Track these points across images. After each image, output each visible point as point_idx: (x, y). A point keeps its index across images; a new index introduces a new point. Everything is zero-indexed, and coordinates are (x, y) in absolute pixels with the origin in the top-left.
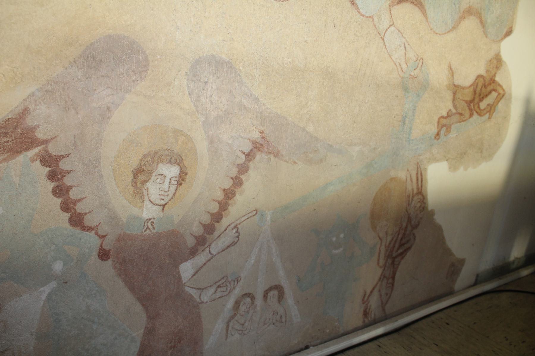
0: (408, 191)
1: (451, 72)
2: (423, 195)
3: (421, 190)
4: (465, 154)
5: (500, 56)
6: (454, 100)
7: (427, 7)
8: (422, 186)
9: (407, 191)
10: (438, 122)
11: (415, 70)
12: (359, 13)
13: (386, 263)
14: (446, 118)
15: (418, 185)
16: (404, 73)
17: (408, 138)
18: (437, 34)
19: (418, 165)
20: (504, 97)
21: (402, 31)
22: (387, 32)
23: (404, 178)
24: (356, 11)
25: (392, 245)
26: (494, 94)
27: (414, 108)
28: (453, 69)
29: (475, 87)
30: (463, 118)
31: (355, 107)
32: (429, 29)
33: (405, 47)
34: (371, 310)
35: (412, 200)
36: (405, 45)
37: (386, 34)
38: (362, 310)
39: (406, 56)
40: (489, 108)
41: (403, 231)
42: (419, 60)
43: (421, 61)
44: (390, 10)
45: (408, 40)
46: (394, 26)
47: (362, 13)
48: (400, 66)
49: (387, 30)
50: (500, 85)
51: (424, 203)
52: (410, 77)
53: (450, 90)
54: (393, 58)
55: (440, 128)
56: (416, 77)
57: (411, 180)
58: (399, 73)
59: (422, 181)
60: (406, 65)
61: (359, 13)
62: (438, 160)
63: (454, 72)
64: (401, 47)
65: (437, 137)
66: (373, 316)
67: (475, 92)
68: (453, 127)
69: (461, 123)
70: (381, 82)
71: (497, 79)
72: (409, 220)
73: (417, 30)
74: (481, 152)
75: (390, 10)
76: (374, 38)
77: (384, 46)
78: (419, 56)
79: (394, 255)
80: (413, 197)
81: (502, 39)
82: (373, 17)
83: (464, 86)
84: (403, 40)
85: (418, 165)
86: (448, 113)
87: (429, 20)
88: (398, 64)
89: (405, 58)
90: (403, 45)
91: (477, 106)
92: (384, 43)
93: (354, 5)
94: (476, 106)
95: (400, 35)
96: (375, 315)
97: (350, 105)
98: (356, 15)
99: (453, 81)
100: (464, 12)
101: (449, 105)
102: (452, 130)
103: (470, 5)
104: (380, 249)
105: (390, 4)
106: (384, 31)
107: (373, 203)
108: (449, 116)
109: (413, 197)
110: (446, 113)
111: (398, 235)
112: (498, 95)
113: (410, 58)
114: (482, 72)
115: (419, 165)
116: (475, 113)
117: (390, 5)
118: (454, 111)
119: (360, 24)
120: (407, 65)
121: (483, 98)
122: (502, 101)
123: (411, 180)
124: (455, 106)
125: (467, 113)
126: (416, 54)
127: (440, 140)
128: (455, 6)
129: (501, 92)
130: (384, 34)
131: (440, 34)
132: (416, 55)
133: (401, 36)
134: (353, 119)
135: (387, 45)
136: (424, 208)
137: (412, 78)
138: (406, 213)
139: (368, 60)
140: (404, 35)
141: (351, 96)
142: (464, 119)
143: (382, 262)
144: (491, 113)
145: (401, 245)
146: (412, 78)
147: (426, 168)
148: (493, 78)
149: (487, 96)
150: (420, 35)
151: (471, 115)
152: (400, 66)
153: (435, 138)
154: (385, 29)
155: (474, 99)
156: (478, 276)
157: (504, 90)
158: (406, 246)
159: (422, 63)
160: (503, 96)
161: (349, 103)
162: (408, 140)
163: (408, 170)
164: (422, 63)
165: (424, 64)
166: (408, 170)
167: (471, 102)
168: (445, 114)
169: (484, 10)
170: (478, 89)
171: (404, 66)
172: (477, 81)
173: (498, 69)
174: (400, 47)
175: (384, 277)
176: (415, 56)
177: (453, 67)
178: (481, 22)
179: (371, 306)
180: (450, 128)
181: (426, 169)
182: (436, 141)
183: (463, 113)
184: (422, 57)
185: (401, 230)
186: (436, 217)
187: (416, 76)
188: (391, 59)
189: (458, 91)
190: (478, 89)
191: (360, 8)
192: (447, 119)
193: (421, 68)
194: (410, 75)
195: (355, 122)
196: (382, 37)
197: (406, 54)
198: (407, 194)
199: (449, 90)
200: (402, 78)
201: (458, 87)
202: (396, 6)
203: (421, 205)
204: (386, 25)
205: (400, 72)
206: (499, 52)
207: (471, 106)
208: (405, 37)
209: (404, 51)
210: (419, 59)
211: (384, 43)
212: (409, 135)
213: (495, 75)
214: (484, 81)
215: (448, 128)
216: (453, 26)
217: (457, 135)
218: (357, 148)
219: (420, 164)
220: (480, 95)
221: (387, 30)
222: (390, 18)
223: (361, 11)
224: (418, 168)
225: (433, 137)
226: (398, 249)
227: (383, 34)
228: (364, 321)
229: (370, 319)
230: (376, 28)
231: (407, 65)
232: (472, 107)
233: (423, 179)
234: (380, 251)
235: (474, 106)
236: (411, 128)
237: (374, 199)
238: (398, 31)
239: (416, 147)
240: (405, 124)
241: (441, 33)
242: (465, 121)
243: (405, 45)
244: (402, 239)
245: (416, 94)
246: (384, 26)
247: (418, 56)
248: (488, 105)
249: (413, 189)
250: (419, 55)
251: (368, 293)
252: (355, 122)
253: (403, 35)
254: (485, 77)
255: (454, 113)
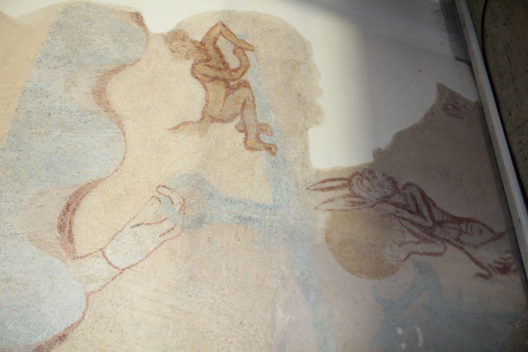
0: (346, 206)
1: (181, 128)
2: (353, 176)
3: (345, 179)
4: (299, 95)
5: (169, 33)
6: (223, 121)
7: (83, 181)
8: (341, 179)
9: (346, 208)
10: (252, 149)
11: (173, 203)
12: (79, 322)
13: (440, 239)
14: (247, 135)
15: (338, 187)
16: (175, 225)
17: (271, 209)
18: (124, 158)
19: (311, 189)
20: (226, 24)
21: (114, 232)
22: (113, 262)
23: (328, 214)
24: (76, 330)
25: (417, 230)
26: (222, 43)
27: (229, 202)
28: (178, 123)
29: (207, 79)
30: (249, 100)
31: (218, 323)
32: (116, 174)
33: (138, 225)
34: (501, 261)
35: (358, 196)
36: (134, 226)
37: (116, 265)
38: (499, 276)
39: (151, 222)
40: (239, 51)
41: (400, 210)
42: (160, 193)
43: (160, 189)
44: (81, 257)
45: (128, 219)
46: (105, 247)
47: (81, 316)
48: (164, 234)
49: (110, 263)
50: (208, 34)
51: (363, 172)
52: (182, 212)
53: (208, 128)
54: (152, 248)
55: (261, 145)
56: (184, 200)
57: (330, 201)
58: (175, 237)
59: (334, 180)
60: (164, 223)
61: (79, 322)
62: (306, 148)
63: (182, 121)
64: (137, 233)
65: (273, 150)
66: (508, 255)
67: (215, 79)
68: (260, 121)
69: (257, 106)
70: (186, 273)
71: (199, 38)
72: (385, 200)
73: (115, 201)
74: (298, 64)
75: (81, 257)
76: (120, 289)
77: (133, 268)
78: (153, 195)
79: (430, 223)
80: (354, 195)
81: (146, 30)
82: (88, 294)
83: (204, 102)
84: (127, 229)
85: (311, 189)
86: (241, 131)
87: (103, 177)
88: (161, 239)
89: (154, 224)
90: (134, 229)
91: (233, 74)
92: (128, 268)
93: (66, 336)
94: (235, 75)
95: (118, 237)
96: (507, 252)
97: (215, 334)
98: (82, 329)
99: (196, 122)
100: (99, 104)
101: (230, 128)
102: (265, 122)
103: (91, 92)
104: (420, 254)
105: (72, 258)
106: (111, 268)
107: (358, 274)
108: (244, 130)
109: (354, 195)
110: (241, 134)
111: (404, 219)
112: (222, 35)
113: (155, 213)
114: (187, 65)
115: (311, 186)
116: (243, 78)
117: (73, 259)
118: (238, 119)
119: (97, 321)
120: (164, 220)
121: (224, 63)
122: (231, 27)
123: (330, 201)
124: (230, 120)
125: (243, 93)
126: (150, 201)
127: (278, 145)
128: (89, 121)
129: (218, 30)
130: (116, 267)
131: (126, 152)
132: (152, 202)
133: (121, 235)
134: (236, 327)
135: (133, 261)
136: (370, 172)
137: (184, 208)
138: (375, 207)
139: (151, 300)
140: (120, 229)
141: (203, 333)
142: (251, 100)
143: (438, 248)
144: (246, 46)
145: (418, 212)
146: (184, 208)
147: (315, 173)
148: (198, 45)
149: (221, 56)
150: (124, 193)
151: (246, 84)
152: (164, 234)
153: (274, 154)
154: (108, 265)
155: (225, 80)
156: (458, 59)
157: (216, 25)
158: (420, 201)
159: (164, 187)
160: (224, 25)
161: (213, 336)
162: (273, 209)
163: (317, 208)
164: (164, 187)
165: (166, 183)
166: (317, 208)
167: (228, 86)
168: (241, 137)
169: (101, 66)
170: (212, 73)
171: (166, 226)
172: (199, 76)
173: (186, 37)
174: (136, 234)
175: (458, 239)
176: (152, 204)
177: (175, 124)
178: (116, 71)
179: (495, 262)
180: (262, 125)
181: (318, 173)
182: (278, 154)
183: (241, 101)
184: (155, 189)
185: (398, 215)
186: (383, 146)
187: (182, 200)
188: (153, 251)
189: (211, 114)
190: (212, 73)
191: (73, 322)
192: (249, 132)
193: (172, 189)
194: (179, 212)
195: (242, 322)
196: (119, 272)
197: (148, 223)
198: (350, 208)
199: (207, 131)
200: (183, 230)
201: (205, 112)
202: (75, 245)
203: (367, 178)
204: (102, 264)
205: (174, 234)
206: (162, 35)
207: (233, 86)
208: (122, 226)
209: (143, 226)
210: (157, 195)
211: (128, 268)
212: (267, 207)
213: (194, 42)
214: (200, 61)
215: (263, 128)
216: (116, 126)
217: (272, 110)
218: (280, 314)
219: (309, 185)
220: (219, 69)
221: (110, 263)
222: (93, 257)
223: (77, 319)
224: (315, 190)
225: (273, 158)
226: (423, 217)
227: (115, 270)
228: (514, 271)
229: (511, 261)
230: (105, 286)
231: (164, 220)
232: (236, 82)
233: (331, 177)
234: (424, 253)
235: (234, 80)
236: (258, 205)
237: (354, 273)
238: (113, 241)
239: (285, 193)
240: (250, 218)
241: (124, 150)
242: (253, 97)
243: (134, 226)
244: (410, 211)
245: (208, 199)
246: (102, 269)
247: (153, 197)
248: (234, 52)
249: (344, 197)
250: (152, 195)
251: (478, 270)
252: (242, 322)
253: (120, 231)
254: (195, 61)
255: (241, 119)
